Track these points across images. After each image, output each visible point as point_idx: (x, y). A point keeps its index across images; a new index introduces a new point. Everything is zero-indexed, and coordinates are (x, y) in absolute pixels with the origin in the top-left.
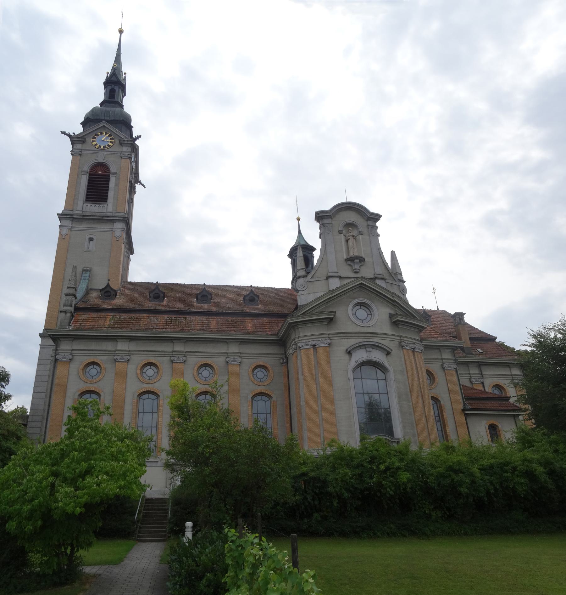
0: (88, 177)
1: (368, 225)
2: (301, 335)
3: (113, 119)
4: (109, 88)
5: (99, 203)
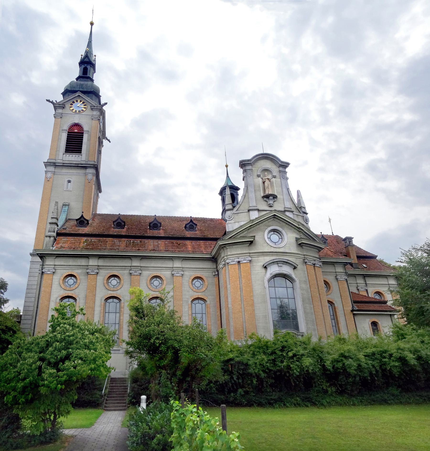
1: (280, 171)
2: (229, 254)
3: (86, 90)
4: (83, 66)
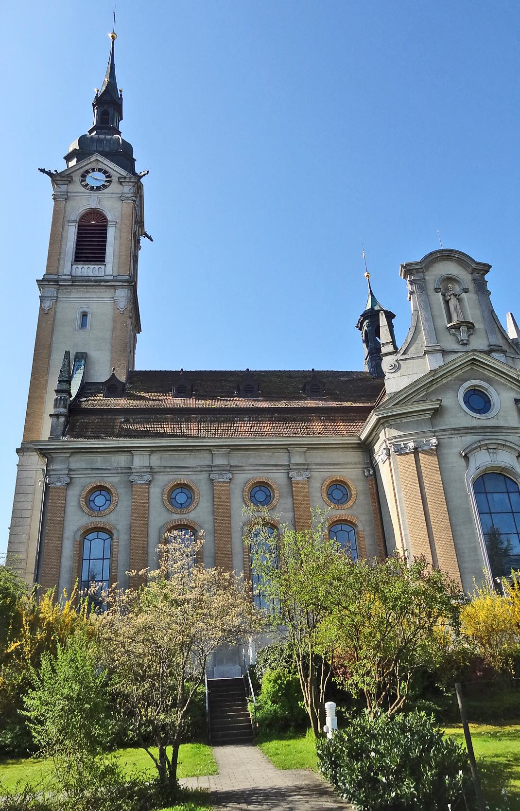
0: (77, 229)
1: (474, 280)
5: (93, 263)
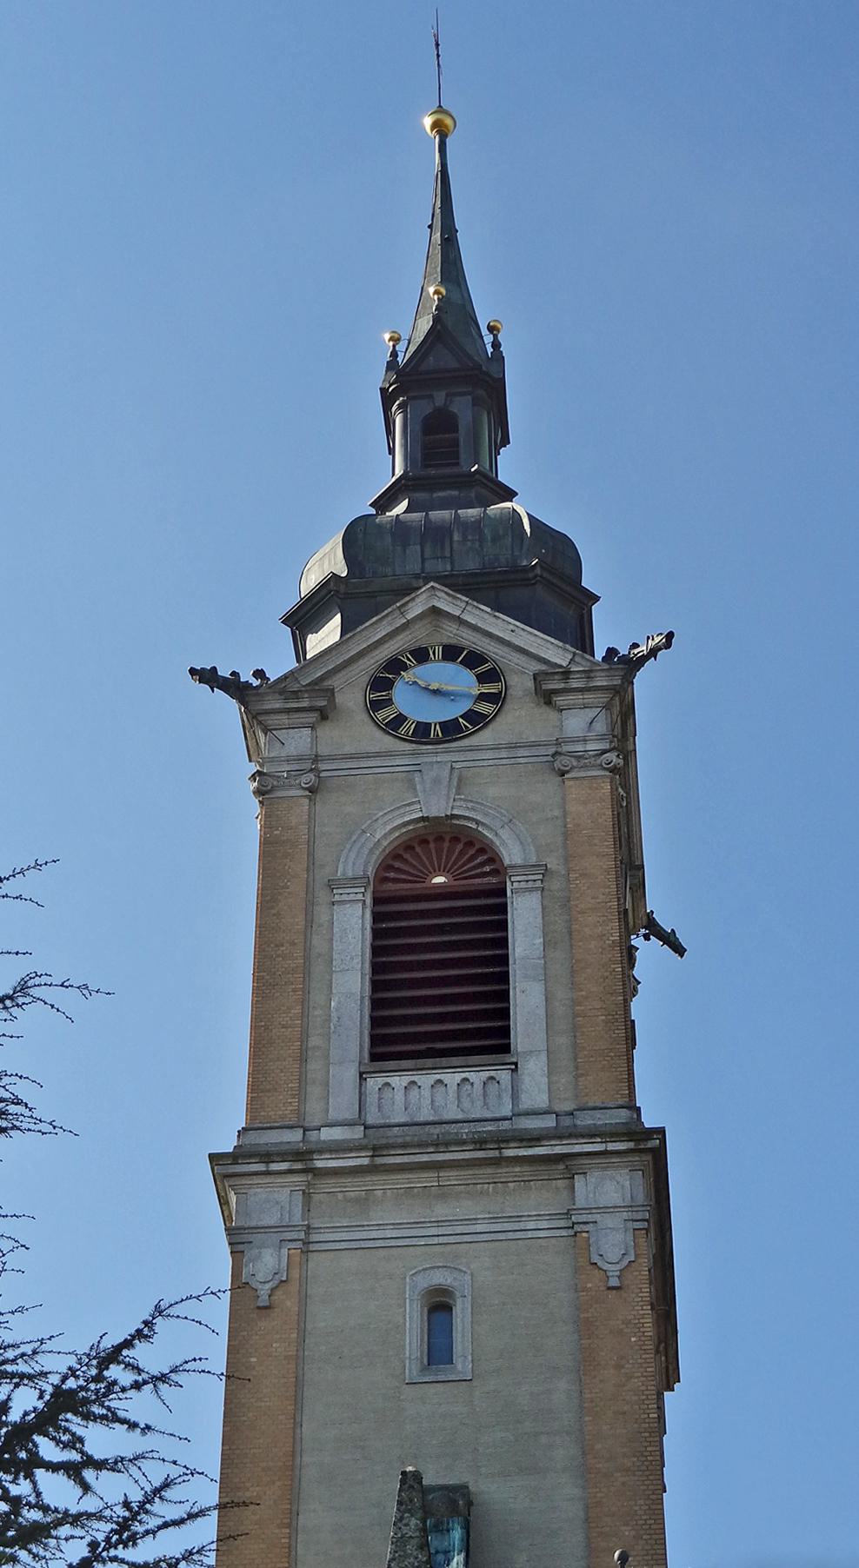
5: (455, 1061)
